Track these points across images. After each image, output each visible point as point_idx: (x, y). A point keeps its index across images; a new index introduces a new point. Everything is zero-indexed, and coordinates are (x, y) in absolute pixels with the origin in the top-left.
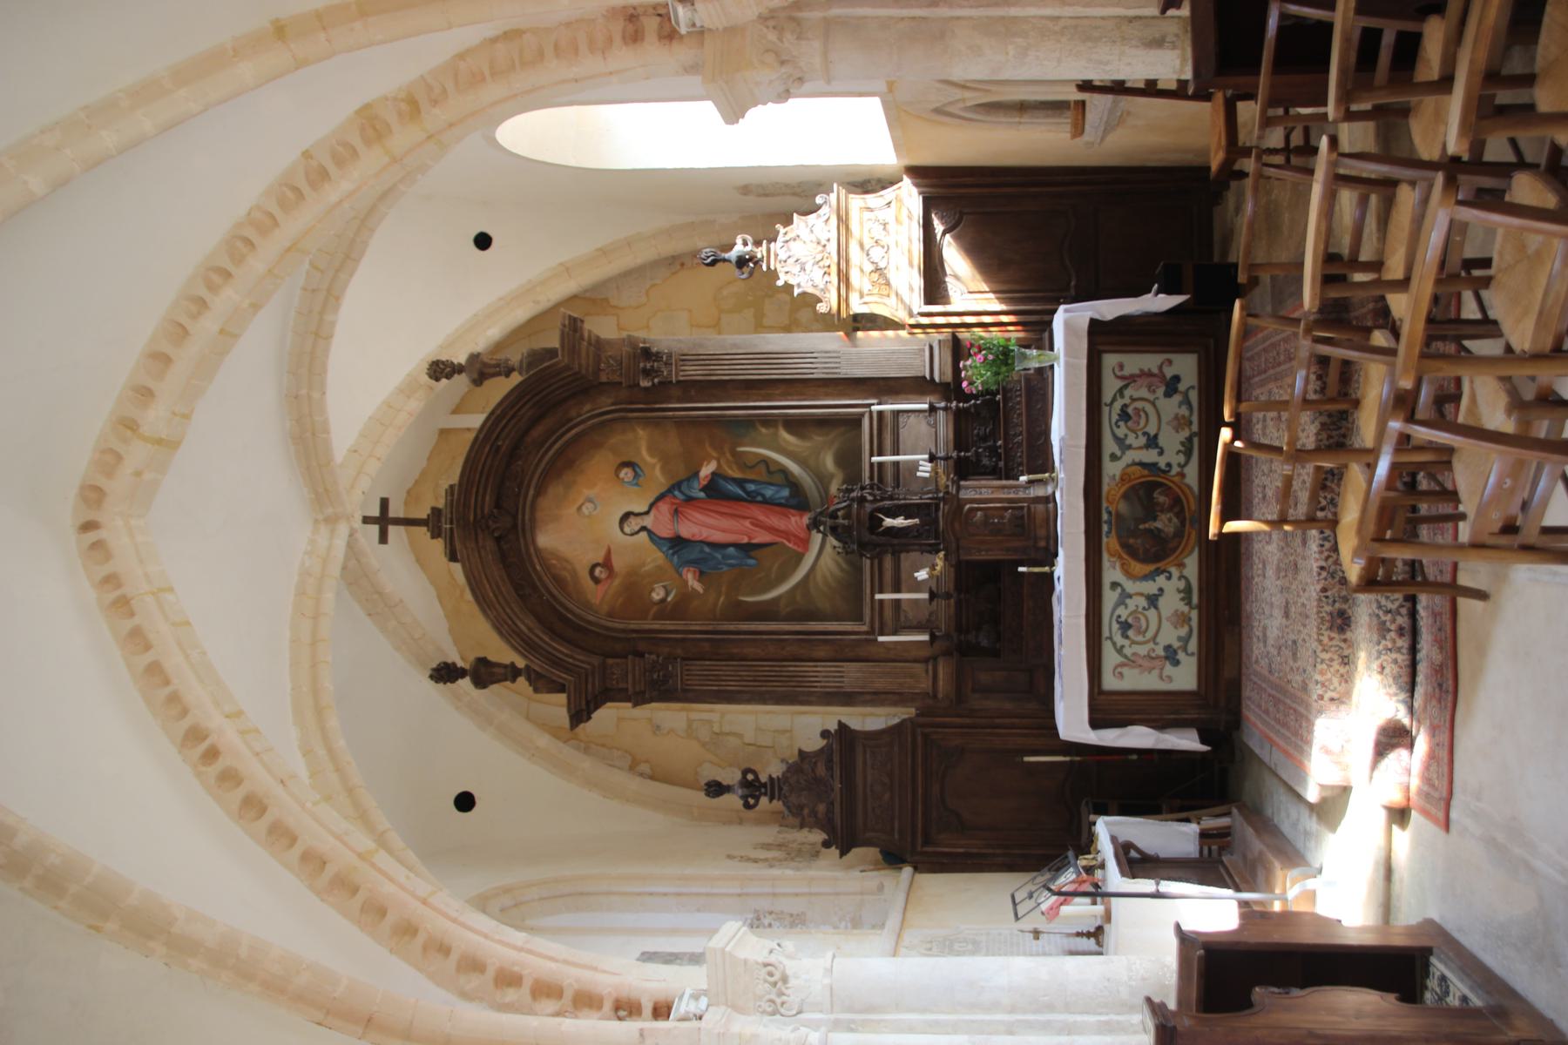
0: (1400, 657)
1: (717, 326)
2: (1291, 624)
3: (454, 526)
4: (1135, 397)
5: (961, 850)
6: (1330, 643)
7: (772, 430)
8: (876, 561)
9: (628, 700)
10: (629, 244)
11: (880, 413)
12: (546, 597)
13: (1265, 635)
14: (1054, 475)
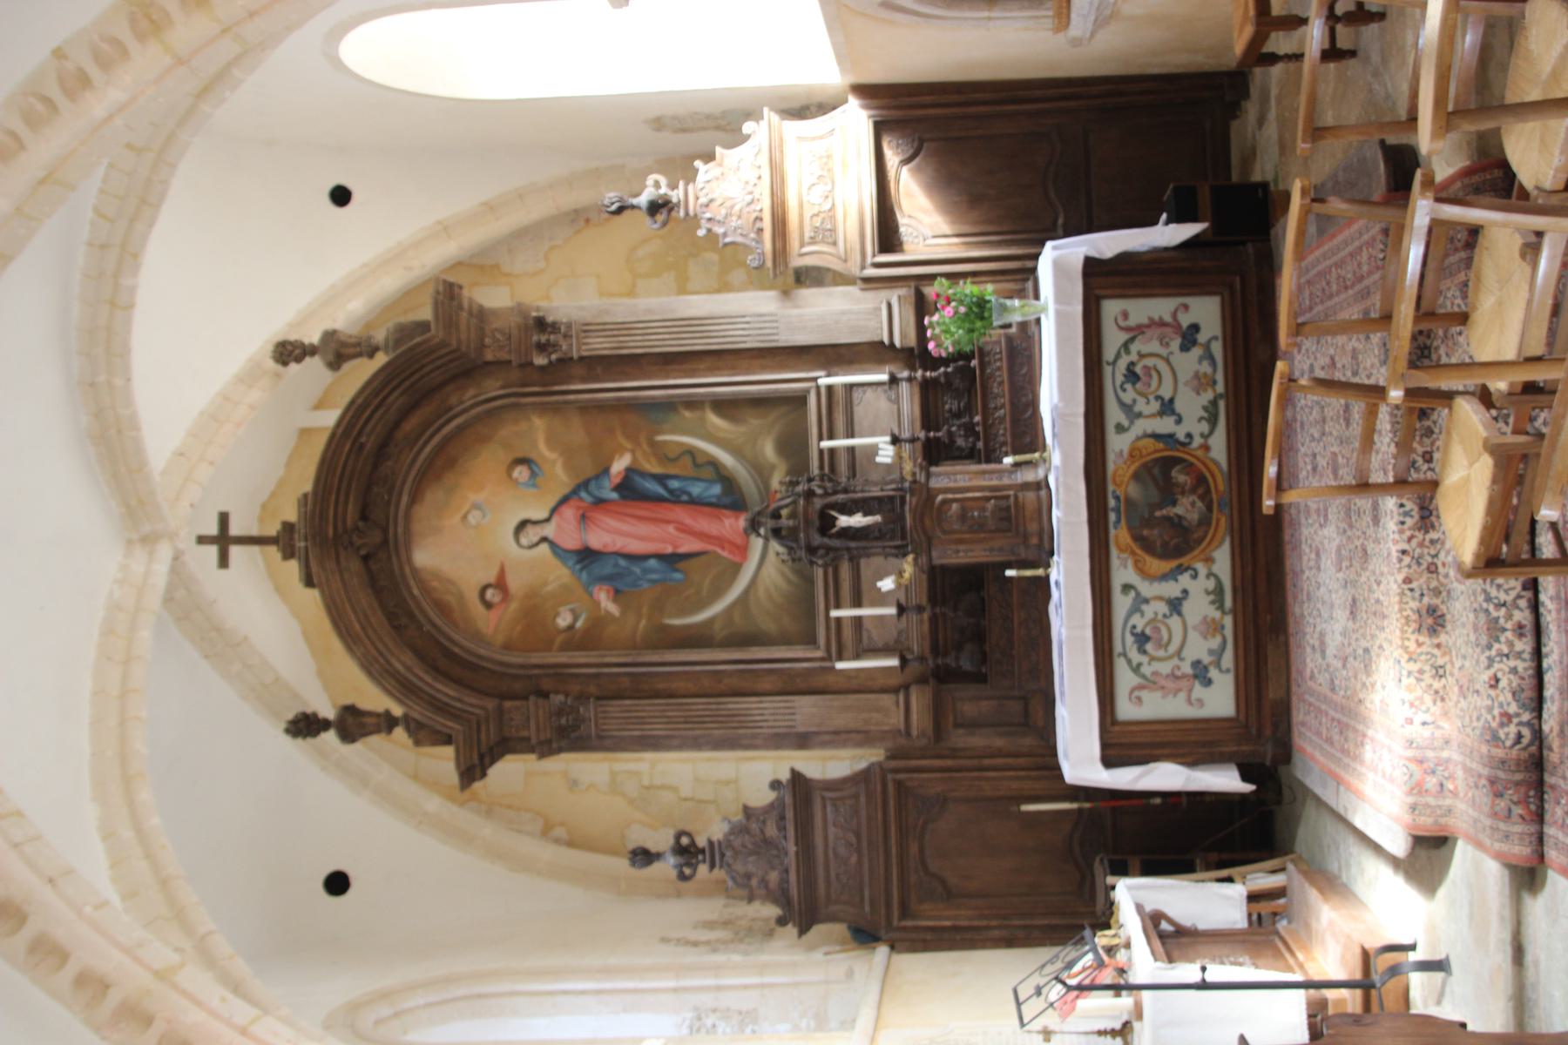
0: (1521, 666)
1: (631, 293)
2: (1361, 627)
3: (309, 544)
4: (1143, 352)
5: (948, 923)
6: (1419, 651)
7: (697, 414)
8: (830, 570)
9: (531, 750)
10: (521, 196)
11: (830, 388)
12: (427, 627)
13: (1323, 643)
14: (1045, 455)
